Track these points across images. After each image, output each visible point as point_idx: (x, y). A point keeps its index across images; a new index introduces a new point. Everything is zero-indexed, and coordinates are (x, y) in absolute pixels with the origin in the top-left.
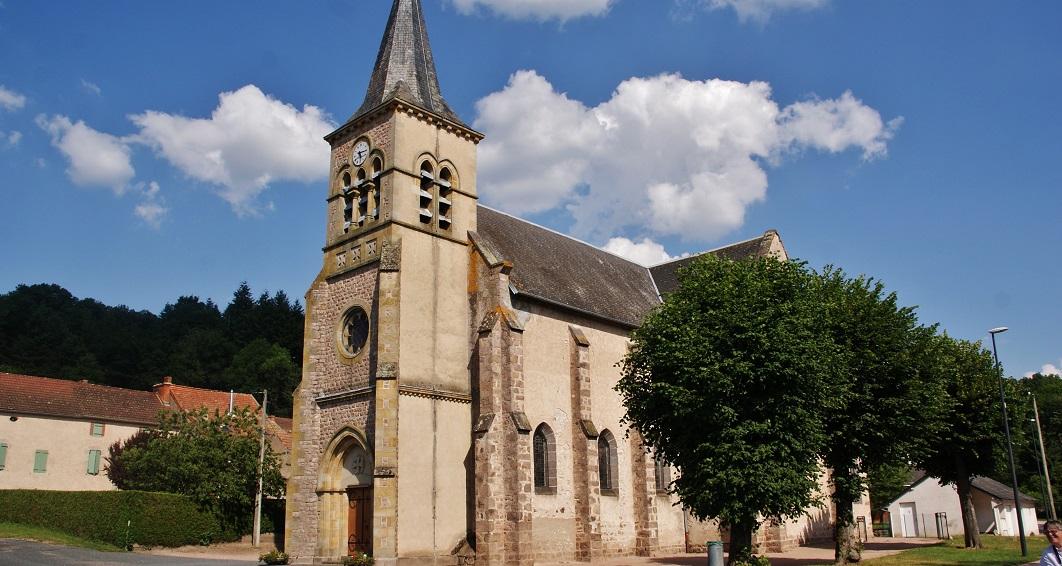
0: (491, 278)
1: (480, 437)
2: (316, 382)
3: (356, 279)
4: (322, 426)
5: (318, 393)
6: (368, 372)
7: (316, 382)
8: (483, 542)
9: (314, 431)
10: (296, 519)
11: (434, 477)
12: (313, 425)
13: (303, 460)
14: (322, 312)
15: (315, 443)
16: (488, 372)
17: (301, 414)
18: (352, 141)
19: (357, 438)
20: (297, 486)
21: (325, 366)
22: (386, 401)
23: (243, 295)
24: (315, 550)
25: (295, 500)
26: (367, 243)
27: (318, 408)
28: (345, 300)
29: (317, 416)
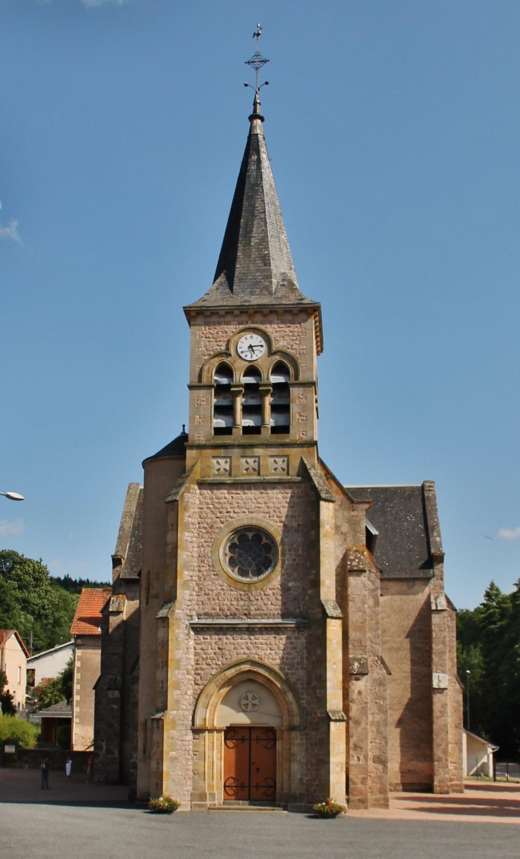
0: (352, 513)
1: (357, 679)
2: (189, 603)
3: (252, 494)
4: (196, 654)
5: (191, 616)
6: (279, 603)
7: (189, 603)
8: (360, 786)
9: (189, 659)
10: (174, 759)
11: (195, 707)
12: (187, 653)
13: (179, 692)
14: (193, 521)
15: (188, 673)
16: (360, 614)
17: (177, 639)
18: (242, 327)
19: (266, 674)
20: (174, 721)
21: (198, 585)
22: (334, 641)
23: (516, 585)
24: (192, 794)
25: (172, 738)
26: (271, 456)
27: (192, 633)
28: (232, 514)
29: (192, 643)
